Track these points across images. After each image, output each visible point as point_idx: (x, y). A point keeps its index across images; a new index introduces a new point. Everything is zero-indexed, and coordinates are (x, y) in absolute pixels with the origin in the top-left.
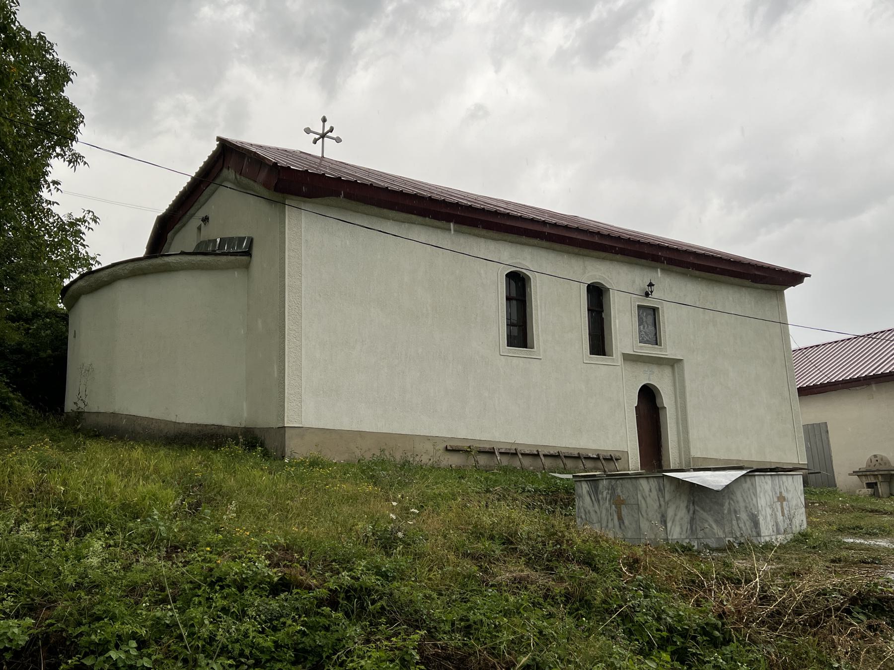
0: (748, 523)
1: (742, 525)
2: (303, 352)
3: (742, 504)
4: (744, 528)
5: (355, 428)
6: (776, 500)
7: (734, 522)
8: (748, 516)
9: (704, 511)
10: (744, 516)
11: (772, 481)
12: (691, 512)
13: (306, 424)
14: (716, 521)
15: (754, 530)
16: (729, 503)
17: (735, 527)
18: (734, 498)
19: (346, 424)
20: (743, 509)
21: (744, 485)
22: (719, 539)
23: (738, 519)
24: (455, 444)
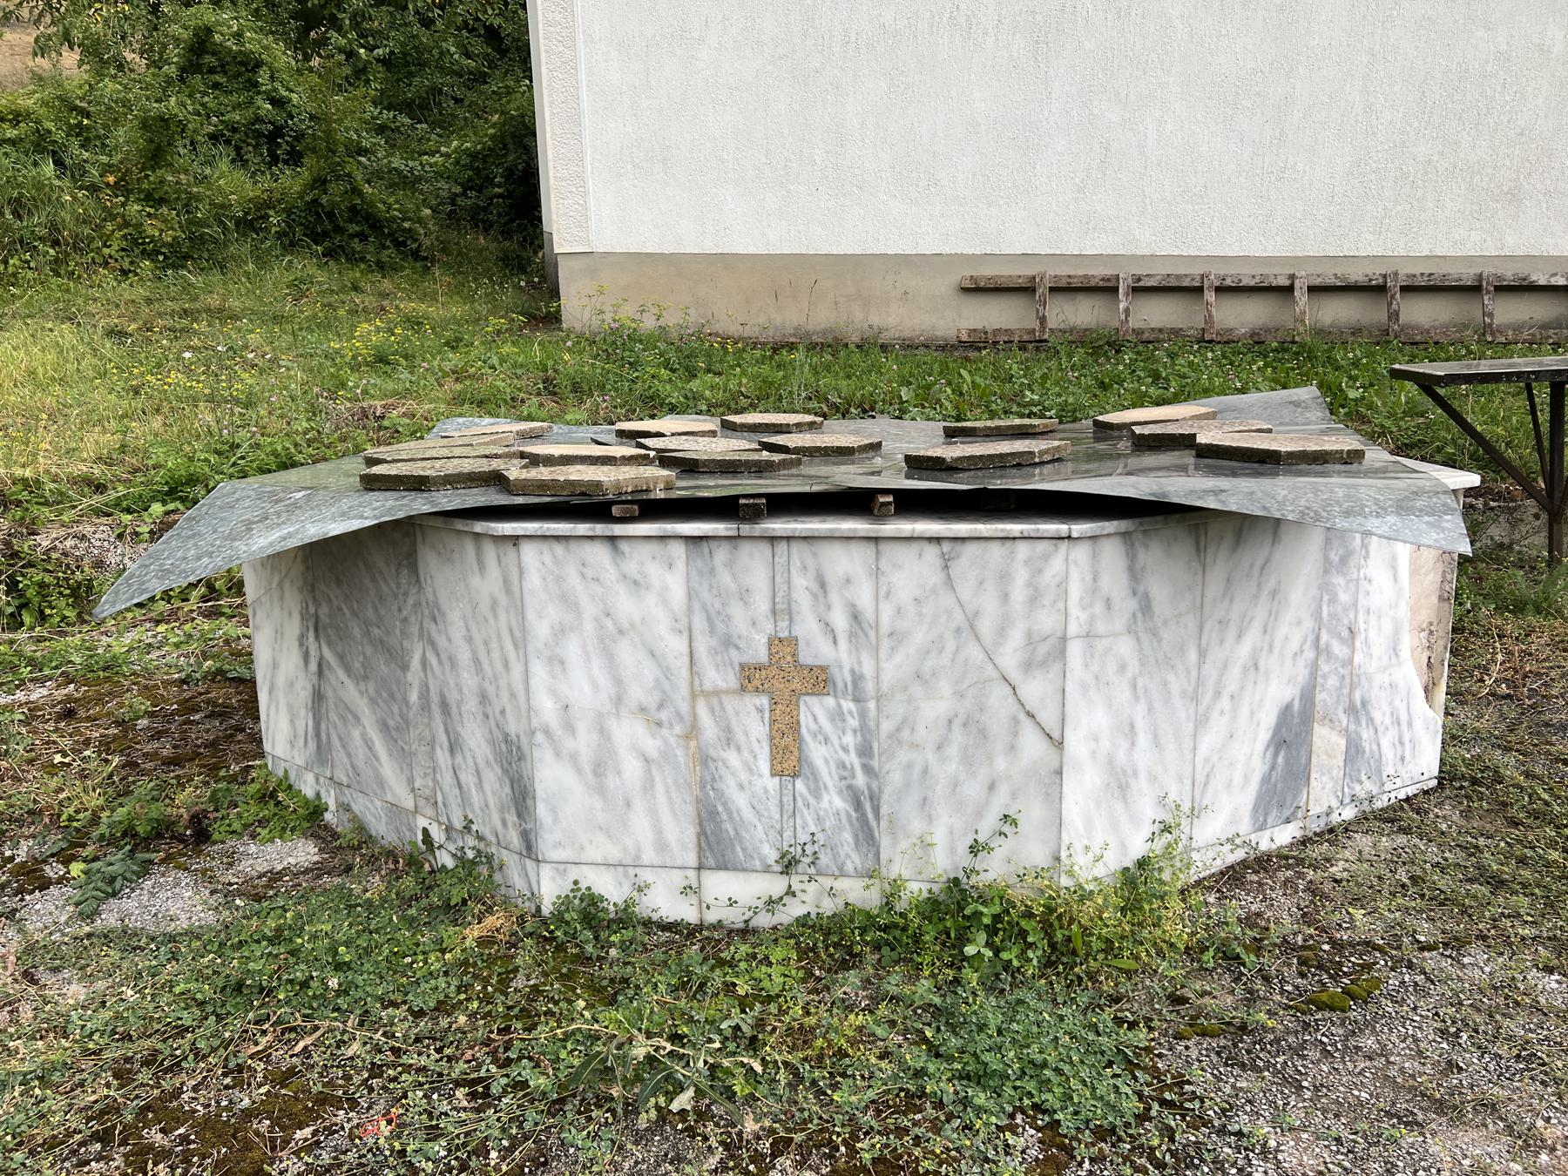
0: (491, 777)
1: (468, 779)
2: (583, 76)
3: (469, 681)
4: (476, 797)
5: (710, 247)
6: (717, 677)
7: (442, 757)
8: (492, 742)
9: (348, 669)
10: (475, 738)
11: (1095, 556)
12: (313, 667)
13: (598, 248)
14: (384, 728)
15: (512, 818)
16: (424, 663)
17: (447, 779)
18: (441, 642)
19: (691, 239)
20: (471, 704)
21: (475, 581)
22: (394, 809)
23: (454, 747)
24: (986, 272)
